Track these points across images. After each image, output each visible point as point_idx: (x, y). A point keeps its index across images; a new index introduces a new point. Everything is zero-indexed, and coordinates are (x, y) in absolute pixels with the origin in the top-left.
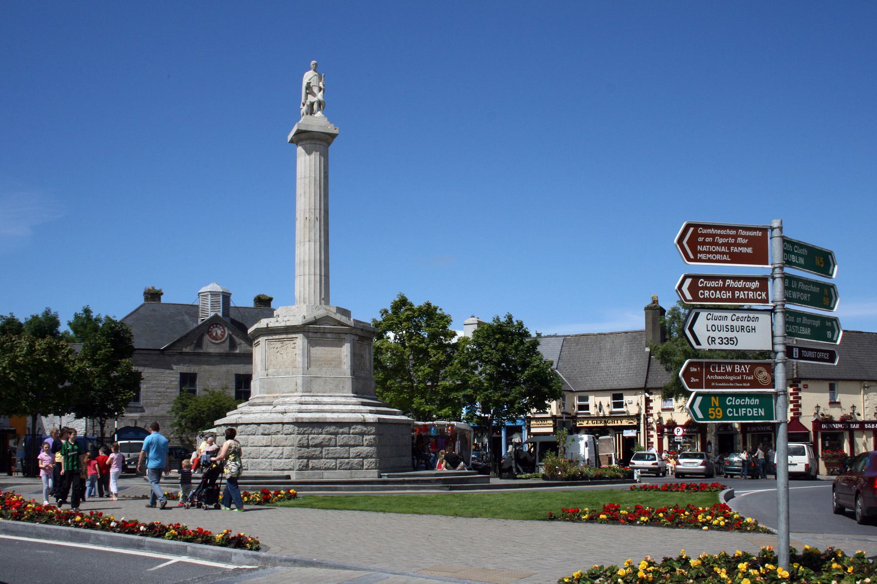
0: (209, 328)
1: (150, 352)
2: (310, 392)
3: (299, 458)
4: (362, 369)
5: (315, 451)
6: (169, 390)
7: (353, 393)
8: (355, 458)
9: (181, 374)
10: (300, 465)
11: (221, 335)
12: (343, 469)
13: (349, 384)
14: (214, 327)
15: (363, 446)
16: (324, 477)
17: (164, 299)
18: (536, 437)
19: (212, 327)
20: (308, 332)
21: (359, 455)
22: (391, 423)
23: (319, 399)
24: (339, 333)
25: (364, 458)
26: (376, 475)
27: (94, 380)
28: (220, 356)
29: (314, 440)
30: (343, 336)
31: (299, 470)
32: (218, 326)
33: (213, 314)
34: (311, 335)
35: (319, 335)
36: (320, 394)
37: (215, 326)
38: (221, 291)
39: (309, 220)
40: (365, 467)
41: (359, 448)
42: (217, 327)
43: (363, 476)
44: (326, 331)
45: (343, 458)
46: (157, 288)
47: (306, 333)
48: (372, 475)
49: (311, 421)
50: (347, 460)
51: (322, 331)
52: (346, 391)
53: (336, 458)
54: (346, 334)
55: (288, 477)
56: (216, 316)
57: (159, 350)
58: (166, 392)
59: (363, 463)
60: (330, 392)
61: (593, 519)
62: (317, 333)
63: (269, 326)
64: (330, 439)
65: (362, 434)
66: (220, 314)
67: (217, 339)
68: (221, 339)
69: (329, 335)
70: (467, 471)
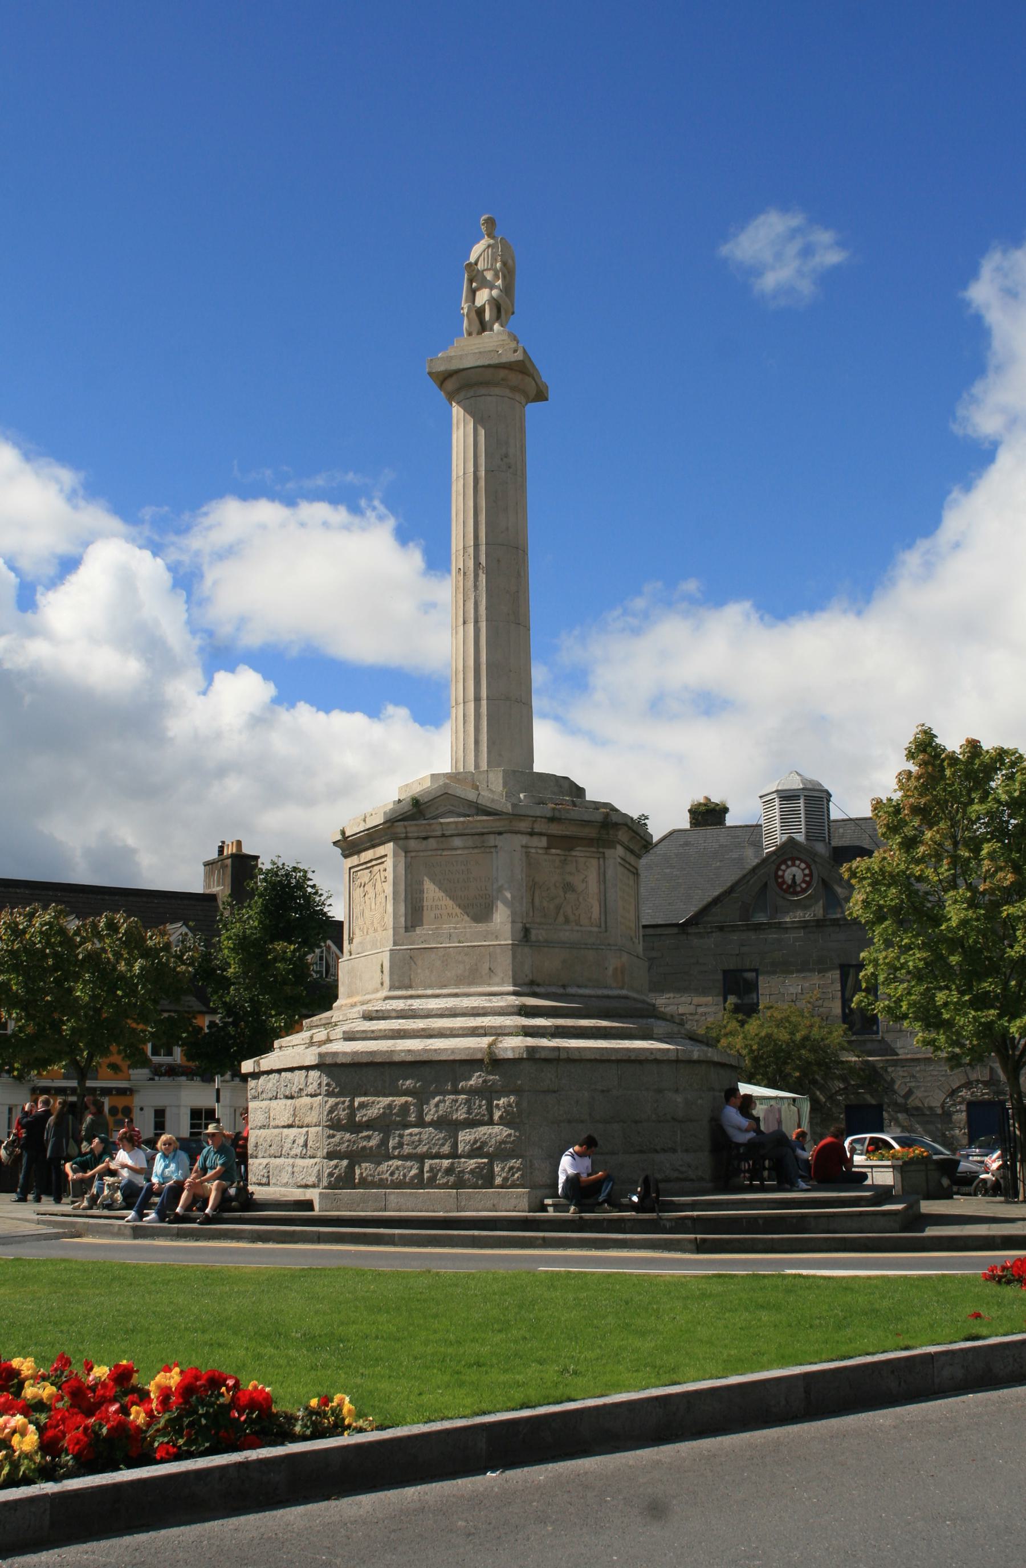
0: (778, 868)
1: (659, 931)
2: (410, 987)
3: (330, 1156)
4: (567, 921)
5: (369, 1138)
6: (701, 1010)
7: (515, 985)
8: (470, 1156)
9: (725, 972)
10: (331, 1175)
11: (804, 881)
12: (439, 1187)
13: (505, 963)
14: (788, 867)
15: (491, 1122)
16: (389, 1207)
17: (730, 820)
18: (215, 1094)
19: (783, 867)
20: (407, 838)
21: (480, 1148)
22: (596, 1060)
23: (417, 1004)
24: (483, 834)
25: (492, 1157)
26: (524, 1203)
27: (52, 982)
28: (804, 928)
29: (364, 1112)
30: (492, 840)
31: (330, 1186)
32: (797, 862)
33: (785, 837)
34: (412, 844)
35: (432, 843)
36: (429, 992)
37: (789, 863)
38: (801, 786)
39: (464, 573)
40: (498, 1181)
41: (483, 1129)
42: (794, 865)
43: (489, 1204)
44: (448, 833)
45: (438, 1156)
46: (715, 799)
47: (401, 842)
48: (513, 1202)
49: (357, 1060)
50: (446, 1163)
51: (439, 833)
52: (497, 979)
53: (421, 1158)
54: (500, 833)
55: (308, 1205)
56: (791, 841)
57: (677, 925)
58: (696, 1014)
59: (492, 1171)
60: (457, 985)
61: (372, 1430)
62: (425, 838)
63: (347, 834)
64: (405, 1107)
65: (488, 1093)
66: (800, 838)
67: (796, 893)
68: (804, 891)
69: (457, 842)
70: (551, 1213)
